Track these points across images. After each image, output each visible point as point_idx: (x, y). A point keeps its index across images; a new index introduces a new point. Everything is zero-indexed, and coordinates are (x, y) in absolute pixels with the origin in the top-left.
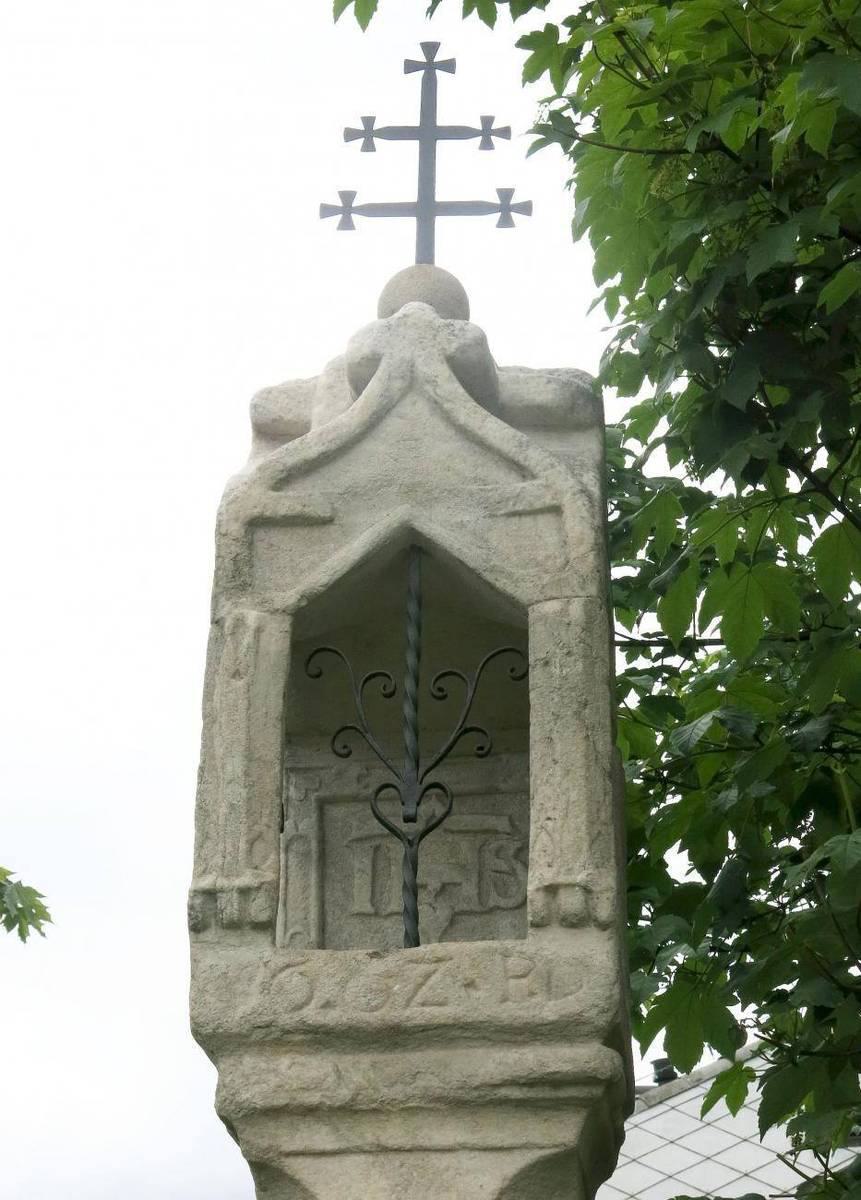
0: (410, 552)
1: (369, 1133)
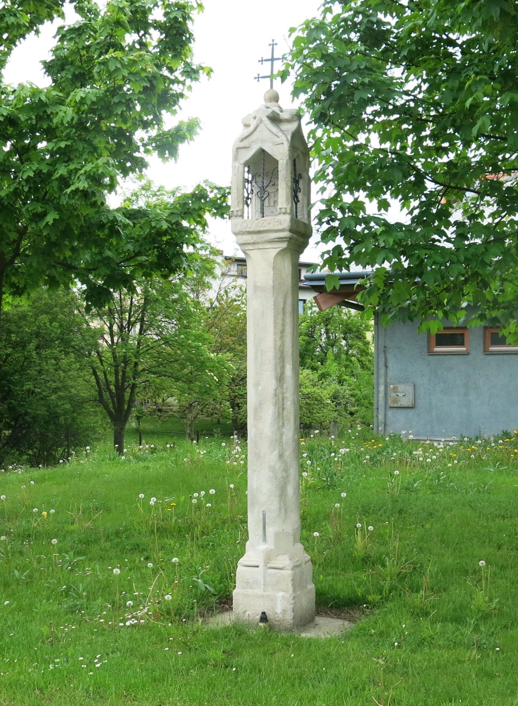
0: (262, 152)
1: (257, 246)
